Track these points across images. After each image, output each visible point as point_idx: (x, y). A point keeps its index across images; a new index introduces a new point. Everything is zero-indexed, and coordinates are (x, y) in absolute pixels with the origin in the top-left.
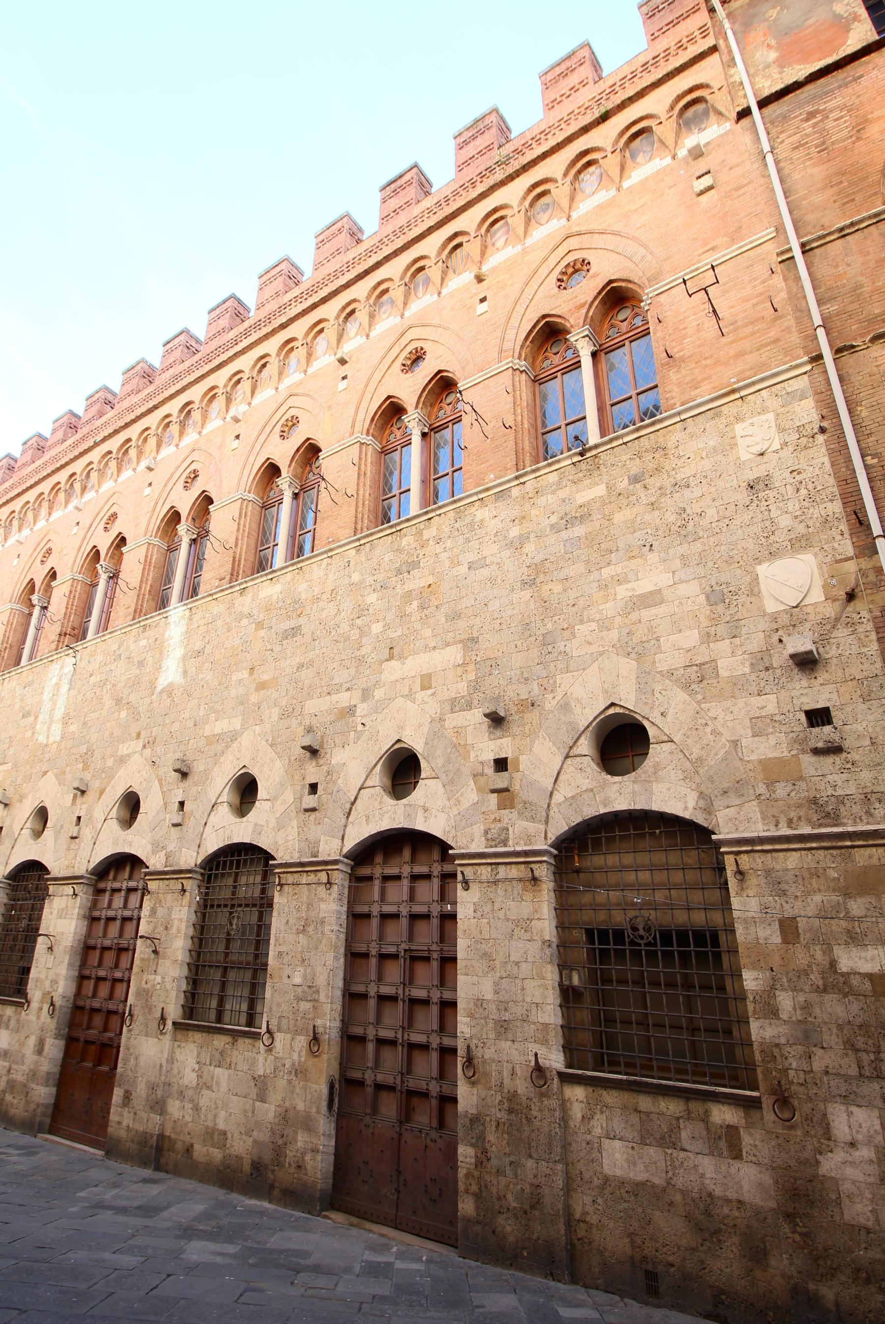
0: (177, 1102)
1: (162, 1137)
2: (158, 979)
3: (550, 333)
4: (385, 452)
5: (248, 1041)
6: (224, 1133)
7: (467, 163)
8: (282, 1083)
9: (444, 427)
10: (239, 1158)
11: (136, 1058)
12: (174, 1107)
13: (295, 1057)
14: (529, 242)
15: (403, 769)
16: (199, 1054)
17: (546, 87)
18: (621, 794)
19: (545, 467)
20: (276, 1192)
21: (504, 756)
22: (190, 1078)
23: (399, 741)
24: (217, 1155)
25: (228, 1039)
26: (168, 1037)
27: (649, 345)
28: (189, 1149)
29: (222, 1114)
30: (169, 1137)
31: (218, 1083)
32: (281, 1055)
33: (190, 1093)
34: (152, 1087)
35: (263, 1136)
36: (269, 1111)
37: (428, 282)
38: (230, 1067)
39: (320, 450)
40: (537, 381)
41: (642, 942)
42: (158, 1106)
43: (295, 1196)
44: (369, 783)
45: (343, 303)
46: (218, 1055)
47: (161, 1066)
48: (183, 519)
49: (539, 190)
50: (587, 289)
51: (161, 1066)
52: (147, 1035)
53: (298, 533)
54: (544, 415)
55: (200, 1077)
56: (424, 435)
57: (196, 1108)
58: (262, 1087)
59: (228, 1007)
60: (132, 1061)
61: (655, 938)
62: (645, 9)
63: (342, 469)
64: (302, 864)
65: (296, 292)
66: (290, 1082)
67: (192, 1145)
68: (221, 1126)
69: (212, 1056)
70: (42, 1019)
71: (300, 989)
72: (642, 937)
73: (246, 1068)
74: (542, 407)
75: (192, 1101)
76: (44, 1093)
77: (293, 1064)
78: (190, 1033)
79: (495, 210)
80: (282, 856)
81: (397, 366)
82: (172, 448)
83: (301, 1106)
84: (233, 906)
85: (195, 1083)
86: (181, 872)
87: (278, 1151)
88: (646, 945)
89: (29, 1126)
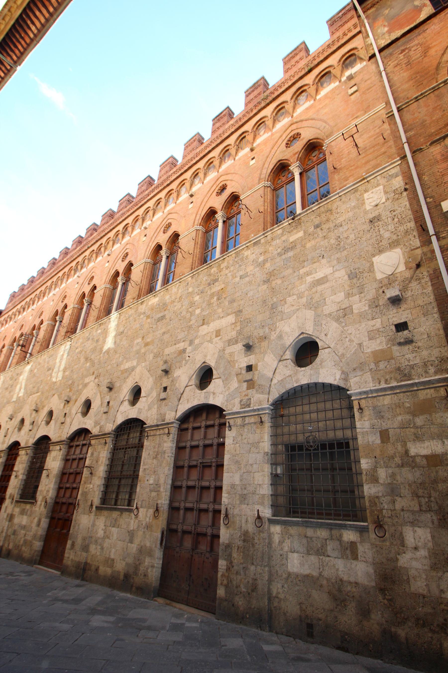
0: (94, 546)
1: (86, 563)
2: (91, 486)
3: (282, 168)
4: (207, 232)
5: (127, 513)
6: (113, 560)
7: (249, 102)
8: (140, 533)
9: (233, 216)
10: (119, 572)
11: (79, 525)
12: (93, 549)
13: (148, 519)
14: (274, 130)
15: (205, 376)
16: (105, 522)
17: (285, 63)
18: (305, 376)
19: (276, 227)
20: (134, 589)
21: (251, 364)
22: (101, 533)
23: (302, 333)
24: (109, 571)
25: (118, 513)
26: (93, 514)
27: (326, 167)
28: (97, 569)
29: (113, 550)
30: (89, 563)
31: (112, 535)
32: (141, 519)
33: (100, 541)
34: (84, 539)
35: (130, 560)
36: (134, 548)
37: (287, 112)
38: (118, 527)
39: (179, 236)
40: (275, 190)
41: (312, 449)
42: (86, 548)
43: (142, 591)
44: (284, 357)
45: (272, 110)
46: (114, 522)
47: (89, 528)
48: (120, 274)
49: (280, 107)
50: (299, 146)
51: (89, 528)
52: (84, 514)
53: (306, 194)
54: (277, 204)
55: (105, 532)
56: (224, 222)
57: (102, 548)
58: (131, 535)
59: (120, 497)
60: (77, 527)
61: (318, 446)
62: (329, 23)
63: (187, 243)
64: (157, 426)
65: (175, 169)
66: (144, 532)
67: (98, 567)
68: (112, 556)
69: (111, 522)
70: (41, 510)
71: (152, 486)
72: (311, 446)
73: (125, 527)
74: (276, 201)
75: (100, 545)
76: (38, 545)
77: (146, 523)
78: (103, 511)
79: (209, 160)
80: (149, 422)
81: (215, 193)
82: (118, 245)
83: (148, 544)
84: (126, 448)
85: (102, 536)
86: (105, 434)
87: (136, 568)
88: (314, 450)
89: (31, 562)
